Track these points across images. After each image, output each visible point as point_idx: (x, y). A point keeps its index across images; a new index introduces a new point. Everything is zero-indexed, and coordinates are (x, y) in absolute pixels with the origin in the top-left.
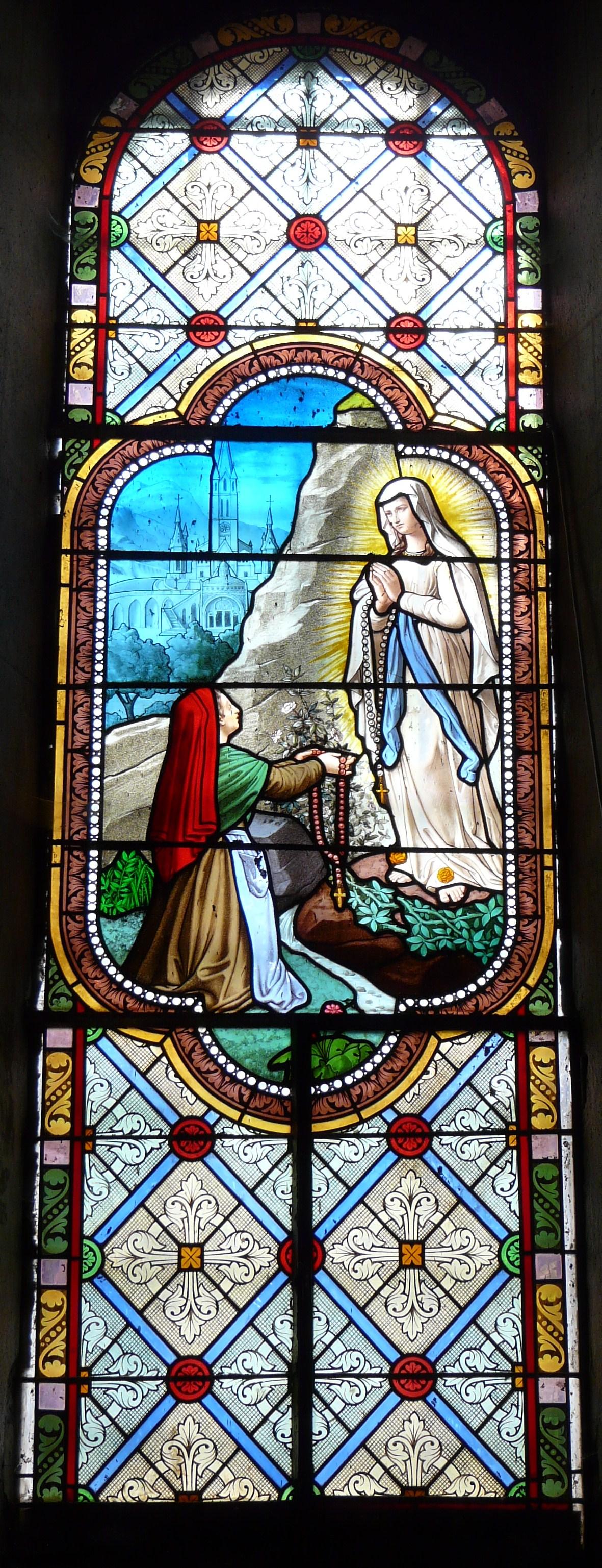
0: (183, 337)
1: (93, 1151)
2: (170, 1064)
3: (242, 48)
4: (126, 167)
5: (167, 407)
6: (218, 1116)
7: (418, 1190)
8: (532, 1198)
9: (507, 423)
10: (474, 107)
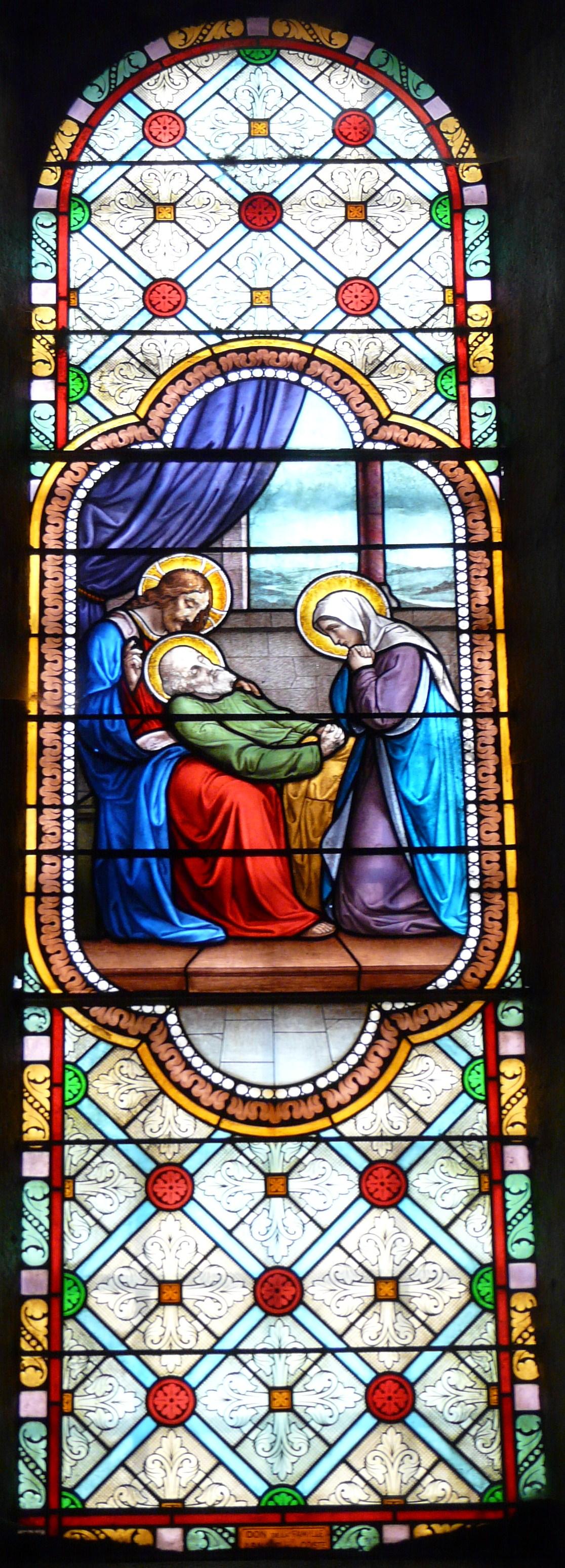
10: (422, 103)
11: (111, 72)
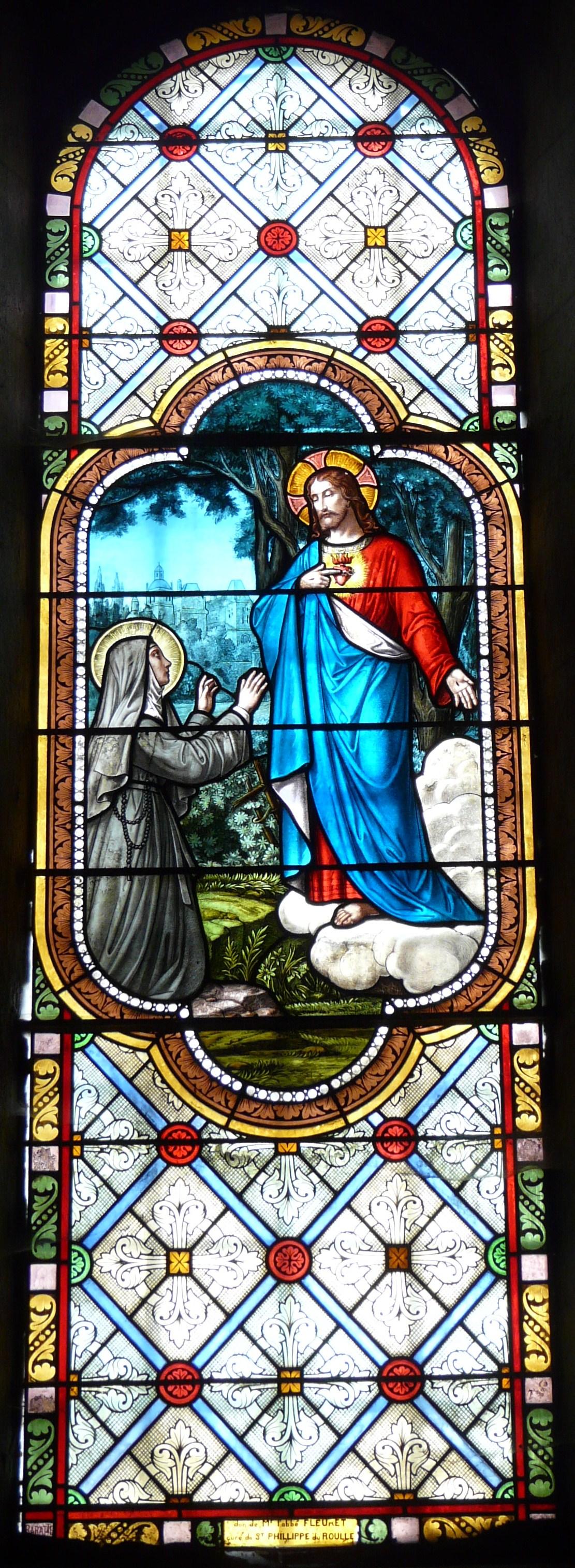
0: (156, 345)
1: (90, 348)
2: (157, 1070)
3: (210, 52)
4: (96, 175)
5: (142, 415)
6: (204, 1122)
7: (403, 1194)
8: (521, 1320)
9: (481, 421)
10: (442, 103)
11: (527, 1322)
